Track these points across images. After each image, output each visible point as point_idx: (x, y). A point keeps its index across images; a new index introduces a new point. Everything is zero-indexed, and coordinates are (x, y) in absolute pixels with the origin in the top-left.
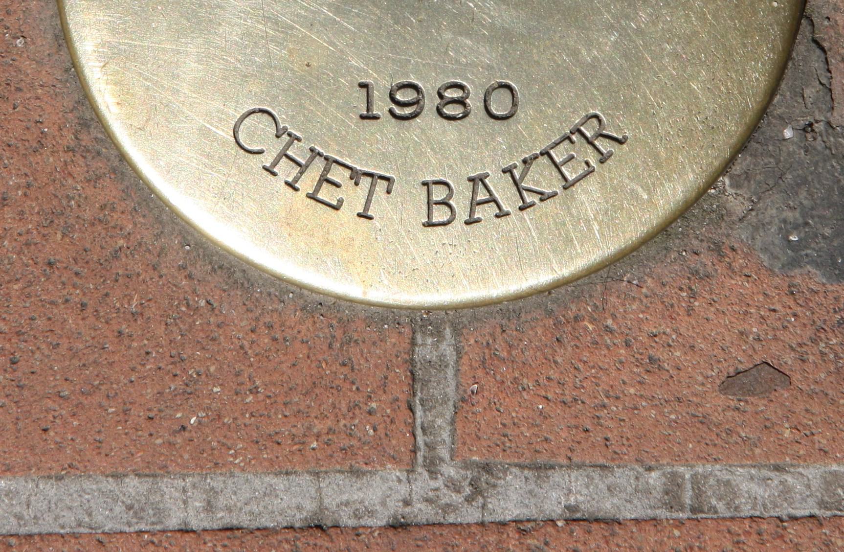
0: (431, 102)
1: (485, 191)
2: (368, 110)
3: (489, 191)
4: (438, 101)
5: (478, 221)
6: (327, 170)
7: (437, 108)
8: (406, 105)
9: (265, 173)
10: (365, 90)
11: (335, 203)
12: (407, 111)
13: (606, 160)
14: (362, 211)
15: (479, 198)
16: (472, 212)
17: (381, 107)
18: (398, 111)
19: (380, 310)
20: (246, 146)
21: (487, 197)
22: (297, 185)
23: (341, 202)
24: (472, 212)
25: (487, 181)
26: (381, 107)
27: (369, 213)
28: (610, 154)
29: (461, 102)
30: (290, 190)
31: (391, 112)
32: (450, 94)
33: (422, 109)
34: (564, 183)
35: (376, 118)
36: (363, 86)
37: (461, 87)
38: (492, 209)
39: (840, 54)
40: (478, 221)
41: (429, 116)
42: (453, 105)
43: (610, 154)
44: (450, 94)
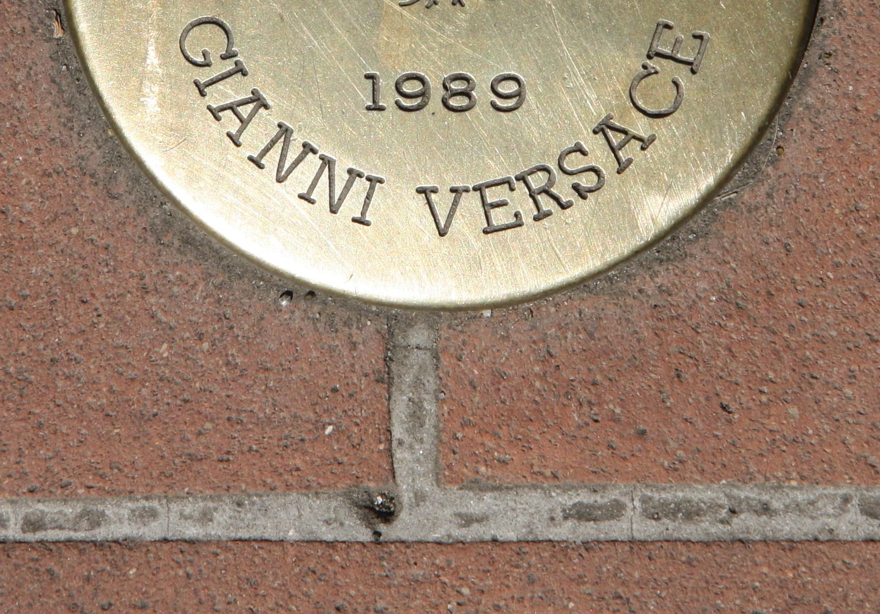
0: (437, 93)
2: (374, 102)
3: (624, 132)
4: (442, 92)
6: (483, 197)
7: (443, 101)
8: (413, 96)
9: (228, 140)
12: (510, 103)
13: (625, 168)
16: (223, 109)
17: (388, 98)
18: (500, 103)
19: (245, 261)
20: (189, 54)
21: (245, 116)
23: (517, 215)
24: (223, 109)
26: (388, 98)
27: (263, 162)
28: (548, 214)
29: (466, 94)
30: (545, 222)
31: (397, 103)
32: (456, 86)
36: (368, 77)
37: (421, 80)
41: (481, 111)
43: (548, 214)
44: (456, 86)
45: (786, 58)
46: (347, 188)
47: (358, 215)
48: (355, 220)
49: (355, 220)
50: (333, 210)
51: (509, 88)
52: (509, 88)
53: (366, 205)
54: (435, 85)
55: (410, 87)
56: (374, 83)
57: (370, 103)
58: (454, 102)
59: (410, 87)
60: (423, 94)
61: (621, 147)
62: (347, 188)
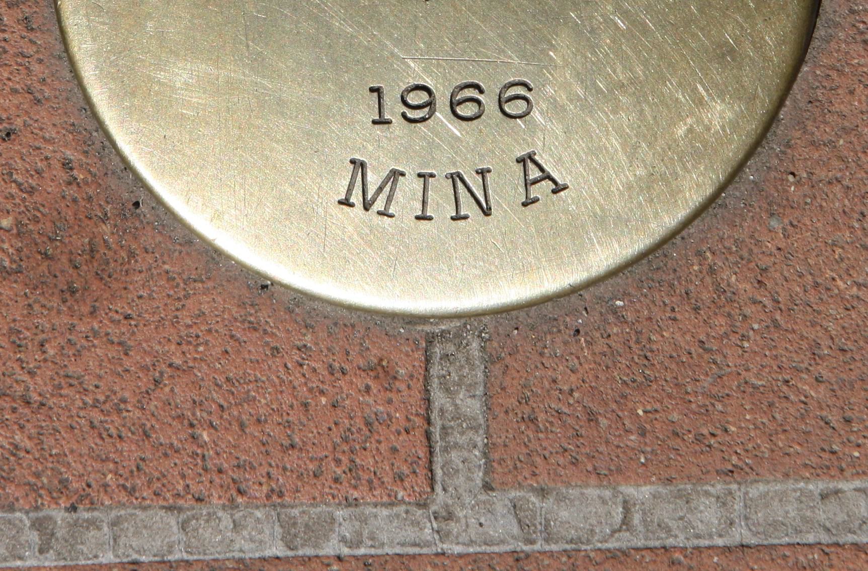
0: (489, 101)
1: (537, 169)
2: (457, 212)
3: (542, 169)
5: (536, 200)
8: (419, 106)
10: (376, 94)
11: (376, 94)
14: (524, 200)
15: (531, 177)
22: (390, 211)
25: (537, 158)
26: (393, 109)
28: (351, 205)
30: (462, 223)
31: (404, 116)
33: (432, 114)
34: (554, 187)
35: (389, 122)
36: (372, 90)
38: (547, 185)
39: (864, 22)
40: (536, 200)
41: (442, 115)
42: (465, 102)
43: (351, 205)
45: (775, 96)
46: (349, 191)
47: (419, 213)
48: (418, 218)
49: (418, 218)
50: (487, 212)
51: (466, 110)
52: (466, 110)
53: (424, 203)
54: (442, 115)
55: (415, 98)
56: (379, 98)
57: (454, 214)
58: (424, 97)
59: (415, 98)
60: (430, 104)
61: (535, 182)
62: (349, 191)
